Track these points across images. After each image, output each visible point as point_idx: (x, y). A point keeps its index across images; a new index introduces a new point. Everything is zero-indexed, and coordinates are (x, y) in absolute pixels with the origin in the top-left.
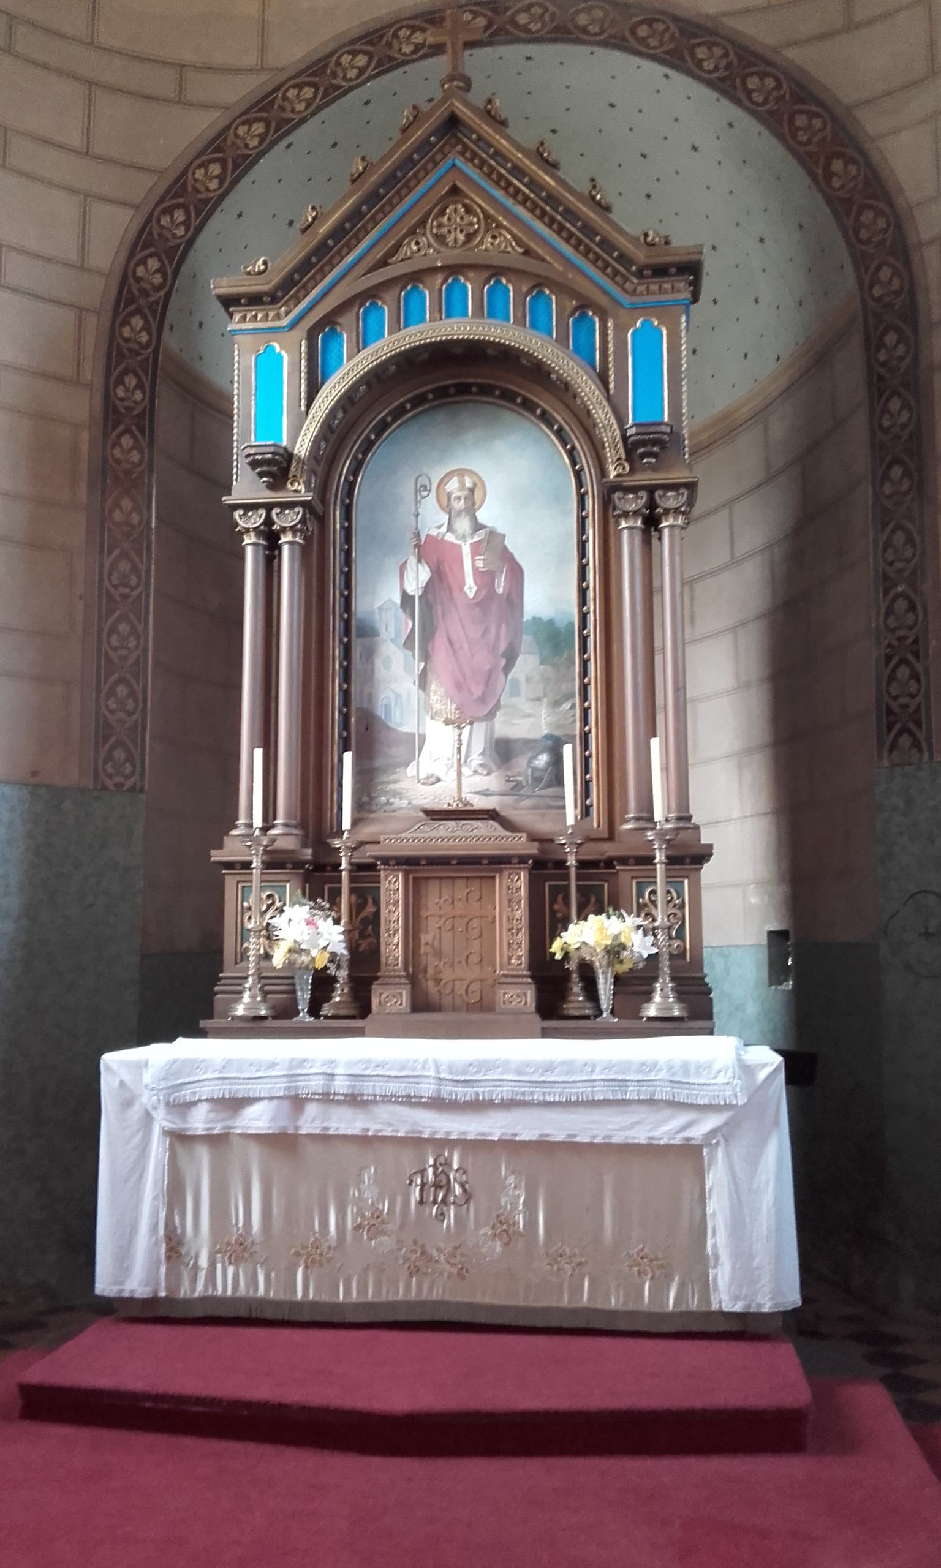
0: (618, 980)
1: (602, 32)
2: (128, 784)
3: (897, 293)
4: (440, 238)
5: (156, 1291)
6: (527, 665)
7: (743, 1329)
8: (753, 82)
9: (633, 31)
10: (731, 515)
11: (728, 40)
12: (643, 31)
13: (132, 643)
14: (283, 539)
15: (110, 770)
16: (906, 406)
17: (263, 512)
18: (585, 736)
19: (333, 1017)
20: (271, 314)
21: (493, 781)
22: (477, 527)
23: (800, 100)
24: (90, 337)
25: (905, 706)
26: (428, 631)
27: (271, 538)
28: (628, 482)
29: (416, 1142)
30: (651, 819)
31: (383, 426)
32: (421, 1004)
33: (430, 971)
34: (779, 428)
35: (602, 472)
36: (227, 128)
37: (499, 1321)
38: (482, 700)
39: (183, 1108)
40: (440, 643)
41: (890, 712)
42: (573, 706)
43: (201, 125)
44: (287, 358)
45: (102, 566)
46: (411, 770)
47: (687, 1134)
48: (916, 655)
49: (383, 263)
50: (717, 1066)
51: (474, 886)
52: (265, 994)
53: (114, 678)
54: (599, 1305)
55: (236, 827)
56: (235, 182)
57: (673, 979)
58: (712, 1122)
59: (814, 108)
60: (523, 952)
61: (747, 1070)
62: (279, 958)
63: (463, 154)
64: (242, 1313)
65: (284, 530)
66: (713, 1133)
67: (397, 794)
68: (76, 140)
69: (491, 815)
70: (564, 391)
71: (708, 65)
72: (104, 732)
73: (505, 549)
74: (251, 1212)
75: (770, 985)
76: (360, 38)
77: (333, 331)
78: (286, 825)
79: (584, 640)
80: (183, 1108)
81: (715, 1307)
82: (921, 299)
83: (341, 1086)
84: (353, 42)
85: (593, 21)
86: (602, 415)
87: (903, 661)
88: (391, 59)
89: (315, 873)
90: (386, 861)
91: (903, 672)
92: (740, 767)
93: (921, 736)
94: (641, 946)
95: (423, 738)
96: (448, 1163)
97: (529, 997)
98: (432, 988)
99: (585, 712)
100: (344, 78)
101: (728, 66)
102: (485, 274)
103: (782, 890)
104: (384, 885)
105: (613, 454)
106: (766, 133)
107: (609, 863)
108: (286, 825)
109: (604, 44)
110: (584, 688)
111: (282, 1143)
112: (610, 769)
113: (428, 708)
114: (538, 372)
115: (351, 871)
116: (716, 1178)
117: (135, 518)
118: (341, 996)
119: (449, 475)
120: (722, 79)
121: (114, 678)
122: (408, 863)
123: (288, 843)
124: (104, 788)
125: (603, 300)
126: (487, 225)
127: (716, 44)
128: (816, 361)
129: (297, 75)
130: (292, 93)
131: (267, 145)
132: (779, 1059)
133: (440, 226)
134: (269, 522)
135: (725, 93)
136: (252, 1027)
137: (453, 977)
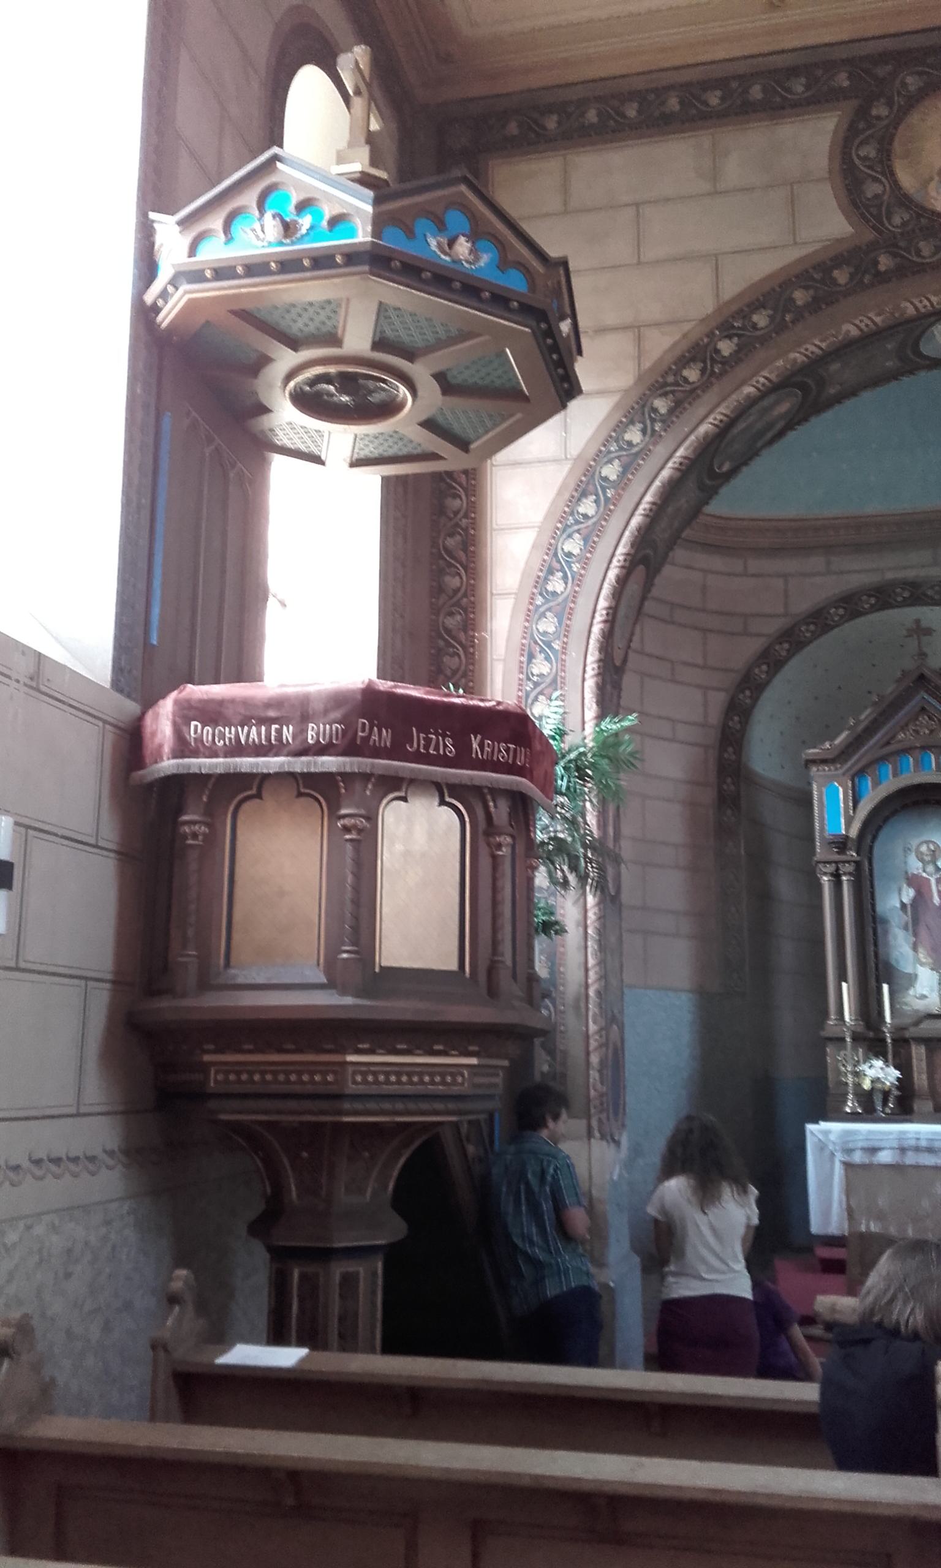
4: (917, 732)
26: (916, 921)
27: (836, 876)
43: (752, 647)
46: (911, 992)
49: (888, 743)
62: (867, 1085)
67: (906, 1004)
80: (849, 1151)
83: (923, 1143)
89: (872, 1042)
95: (916, 975)
111: (896, 1168)
115: (893, 1045)
119: (922, 843)
123: (859, 1029)
131: (791, 654)
134: (838, 869)
136: (854, 1117)
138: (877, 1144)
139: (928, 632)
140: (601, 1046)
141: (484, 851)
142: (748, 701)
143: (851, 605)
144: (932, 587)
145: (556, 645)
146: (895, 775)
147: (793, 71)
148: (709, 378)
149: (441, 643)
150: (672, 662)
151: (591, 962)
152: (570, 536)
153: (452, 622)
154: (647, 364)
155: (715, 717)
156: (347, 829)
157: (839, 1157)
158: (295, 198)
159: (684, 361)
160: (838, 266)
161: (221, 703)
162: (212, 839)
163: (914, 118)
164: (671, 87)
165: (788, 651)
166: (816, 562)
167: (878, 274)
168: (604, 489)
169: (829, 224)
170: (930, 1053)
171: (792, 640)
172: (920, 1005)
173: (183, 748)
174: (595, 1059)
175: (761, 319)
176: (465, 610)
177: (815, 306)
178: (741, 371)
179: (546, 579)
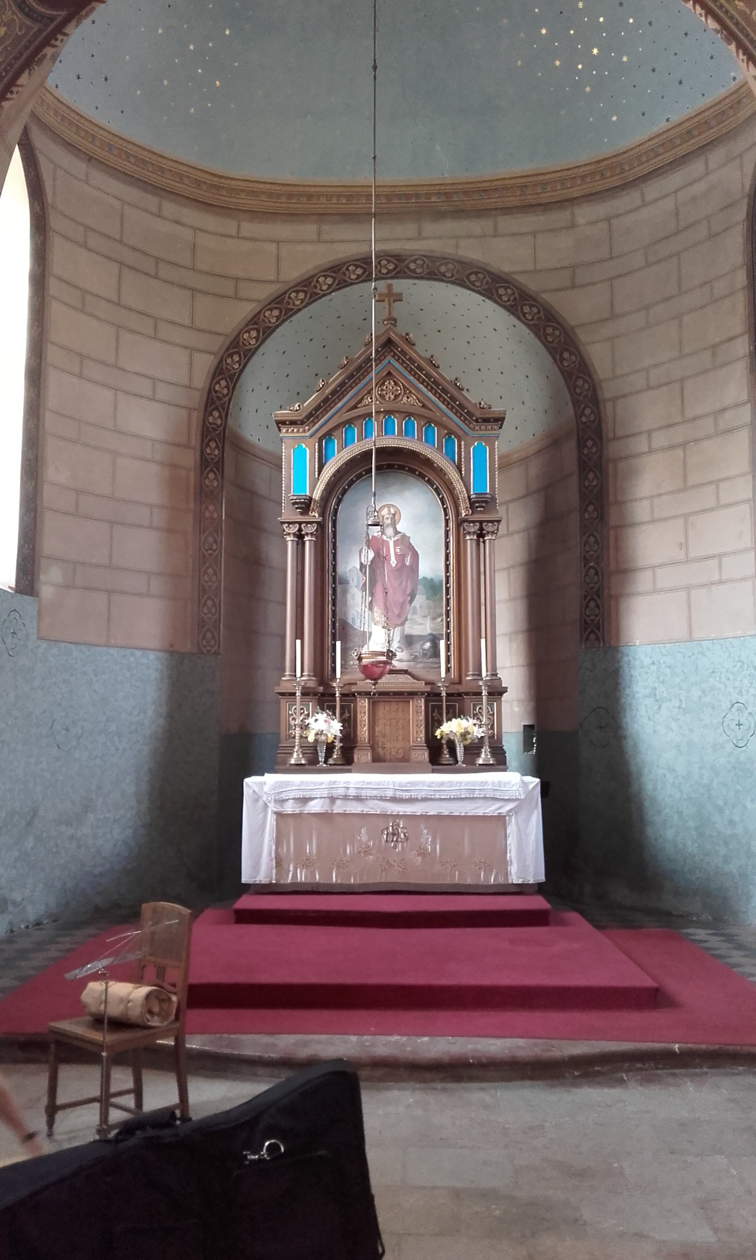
0: (466, 748)
1: (452, 277)
2: (213, 650)
3: (593, 422)
5: (271, 880)
6: (420, 600)
7: (521, 890)
8: (526, 309)
9: (468, 278)
10: (507, 509)
11: (516, 288)
12: (473, 278)
13: (214, 578)
14: (306, 538)
15: (205, 643)
16: (596, 477)
17: (297, 526)
18: (448, 635)
19: (334, 765)
20: (301, 430)
22: (397, 532)
23: (549, 321)
24: (194, 422)
25: (593, 620)
26: (373, 582)
27: (300, 536)
28: (471, 518)
29: (385, 816)
30: (480, 675)
31: (351, 483)
32: (377, 759)
33: (380, 744)
34: (534, 469)
35: (458, 514)
36: (259, 313)
37: (418, 889)
38: (399, 616)
39: (283, 801)
41: (586, 622)
42: (442, 620)
43: (246, 310)
44: (308, 452)
45: (200, 540)
47: (499, 811)
48: (598, 596)
49: (355, 407)
50: (513, 783)
51: (401, 704)
52: (304, 754)
53: (206, 596)
54: (463, 882)
55: (285, 676)
57: (490, 747)
58: (511, 806)
59: (555, 325)
60: (423, 735)
61: (525, 784)
62: (311, 738)
63: (393, 357)
64: (309, 889)
65: (307, 534)
66: (511, 810)
68: (187, 321)
69: (405, 672)
70: (440, 472)
71: (505, 298)
72: (202, 624)
73: (410, 544)
75: (524, 751)
76: (329, 269)
77: (330, 438)
78: (309, 675)
79: (447, 589)
81: (510, 882)
82: (603, 425)
83: (352, 792)
84: (325, 271)
85: (448, 270)
86: (459, 486)
87: (592, 599)
88: (345, 281)
89: (323, 697)
90: (360, 693)
91: (592, 604)
92: (510, 640)
93: (600, 634)
94: (478, 732)
95: (370, 634)
96: (398, 825)
98: (380, 751)
99: (448, 624)
100: (321, 290)
101: (515, 299)
102: (403, 415)
103: (531, 705)
104: (359, 704)
106: (532, 335)
107: (460, 695)
108: (309, 675)
109: (453, 283)
110: (448, 612)
111: (325, 817)
113: (373, 619)
114: (428, 462)
115: (340, 698)
116: (511, 829)
117: (215, 516)
118: (344, 754)
119: (384, 507)
120: (512, 306)
121: (206, 596)
123: (311, 684)
124: (203, 653)
125: (460, 433)
126: (405, 391)
127: (509, 288)
128: (553, 443)
129: (297, 285)
130: (293, 295)
131: (281, 321)
132: (534, 782)
133: (382, 390)
134: (300, 530)
135: (513, 314)
136: (299, 768)
137: (391, 747)
138: (307, 794)
139: (399, 298)
142: (236, 366)
143: (340, 275)
144: (415, 261)
150: (156, 319)
155: (201, 380)
165: (278, 318)
166: (309, 229)
170: (373, 705)
171: (283, 306)
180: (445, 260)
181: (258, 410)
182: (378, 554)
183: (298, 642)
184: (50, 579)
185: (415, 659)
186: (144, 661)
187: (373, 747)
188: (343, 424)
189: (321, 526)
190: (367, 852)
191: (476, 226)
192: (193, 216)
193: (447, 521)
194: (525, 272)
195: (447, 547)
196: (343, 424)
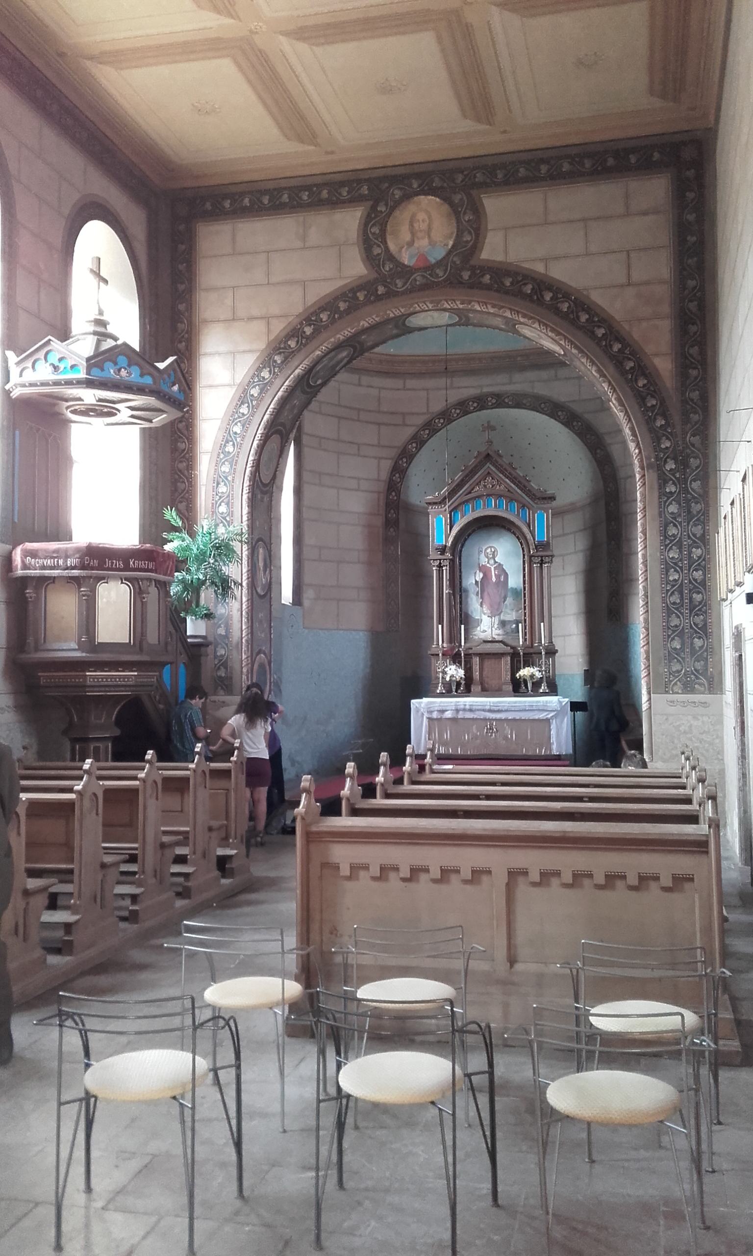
4: (485, 486)
6: (509, 600)
21: (500, 632)
22: (496, 562)
26: (482, 591)
27: (440, 566)
29: (485, 720)
38: (497, 610)
39: (431, 712)
40: (486, 593)
43: (410, 431)
49: (470, 493)
56: (421, 448)
62: (448, 679)
71: (562, 417)
74: (447, 736)
80: (431, 712)
83: (468, 707)
86: (529, 536)
89: (456, 659)
94: (538, 675)
97: (511, 688)
103: (587, 658)
105: (532, 547)
107: (531, 654)
110: (525, 607)
111: (454, 720)
112: (532, 631)
116: (553, 727)
118: (466, 687)
122: (480, 655)
128: (594, 501)
131: (430, 436)
136: (441, 695)
137: (493, 683)
138: (444, 708)
140: (247, 665)
141: (138, 600)
143: (464, 407)
145: (230, 478)
146: (473, 510)
147: (342, 184)
148: (301, 346)
149: (177, 477)
151: (244, 627)
152: (236, 424)
153: (182, 466)
154: (272, 337)
155: (384, 475)
156: (84, 596)
157: (426, 715)
158: (58, 356)
159: (289, 337)
160: (360, 290)
161: (37, 551)
162: (38, 599)
163: (397, 213)
164: (285, 188)
167: (378, 295)
168: (252, 401)
169: (356, 268)
171: (431, 428)
172: (483, 636)
173: (25, 567)
174: (245, 670)
175: (324, 316)
176: (188, 460)
177: (348, 311)
178: (315, 343)
179: (225, 445)
180: (525, 395)
181: (421, 487)
182: (485, 575)
183: (440, 626)
184: (308, 595)
185: (507, 634)
186: (358, 637)
187: (482, 684)
188: (464, 502)
189: (452, 561)
190: (476, 739)
191: (544, 374)
192: (377, 381)
193: (524, 555)
194: (574, 401)
195: (524, 570)
196: (464, 502)
